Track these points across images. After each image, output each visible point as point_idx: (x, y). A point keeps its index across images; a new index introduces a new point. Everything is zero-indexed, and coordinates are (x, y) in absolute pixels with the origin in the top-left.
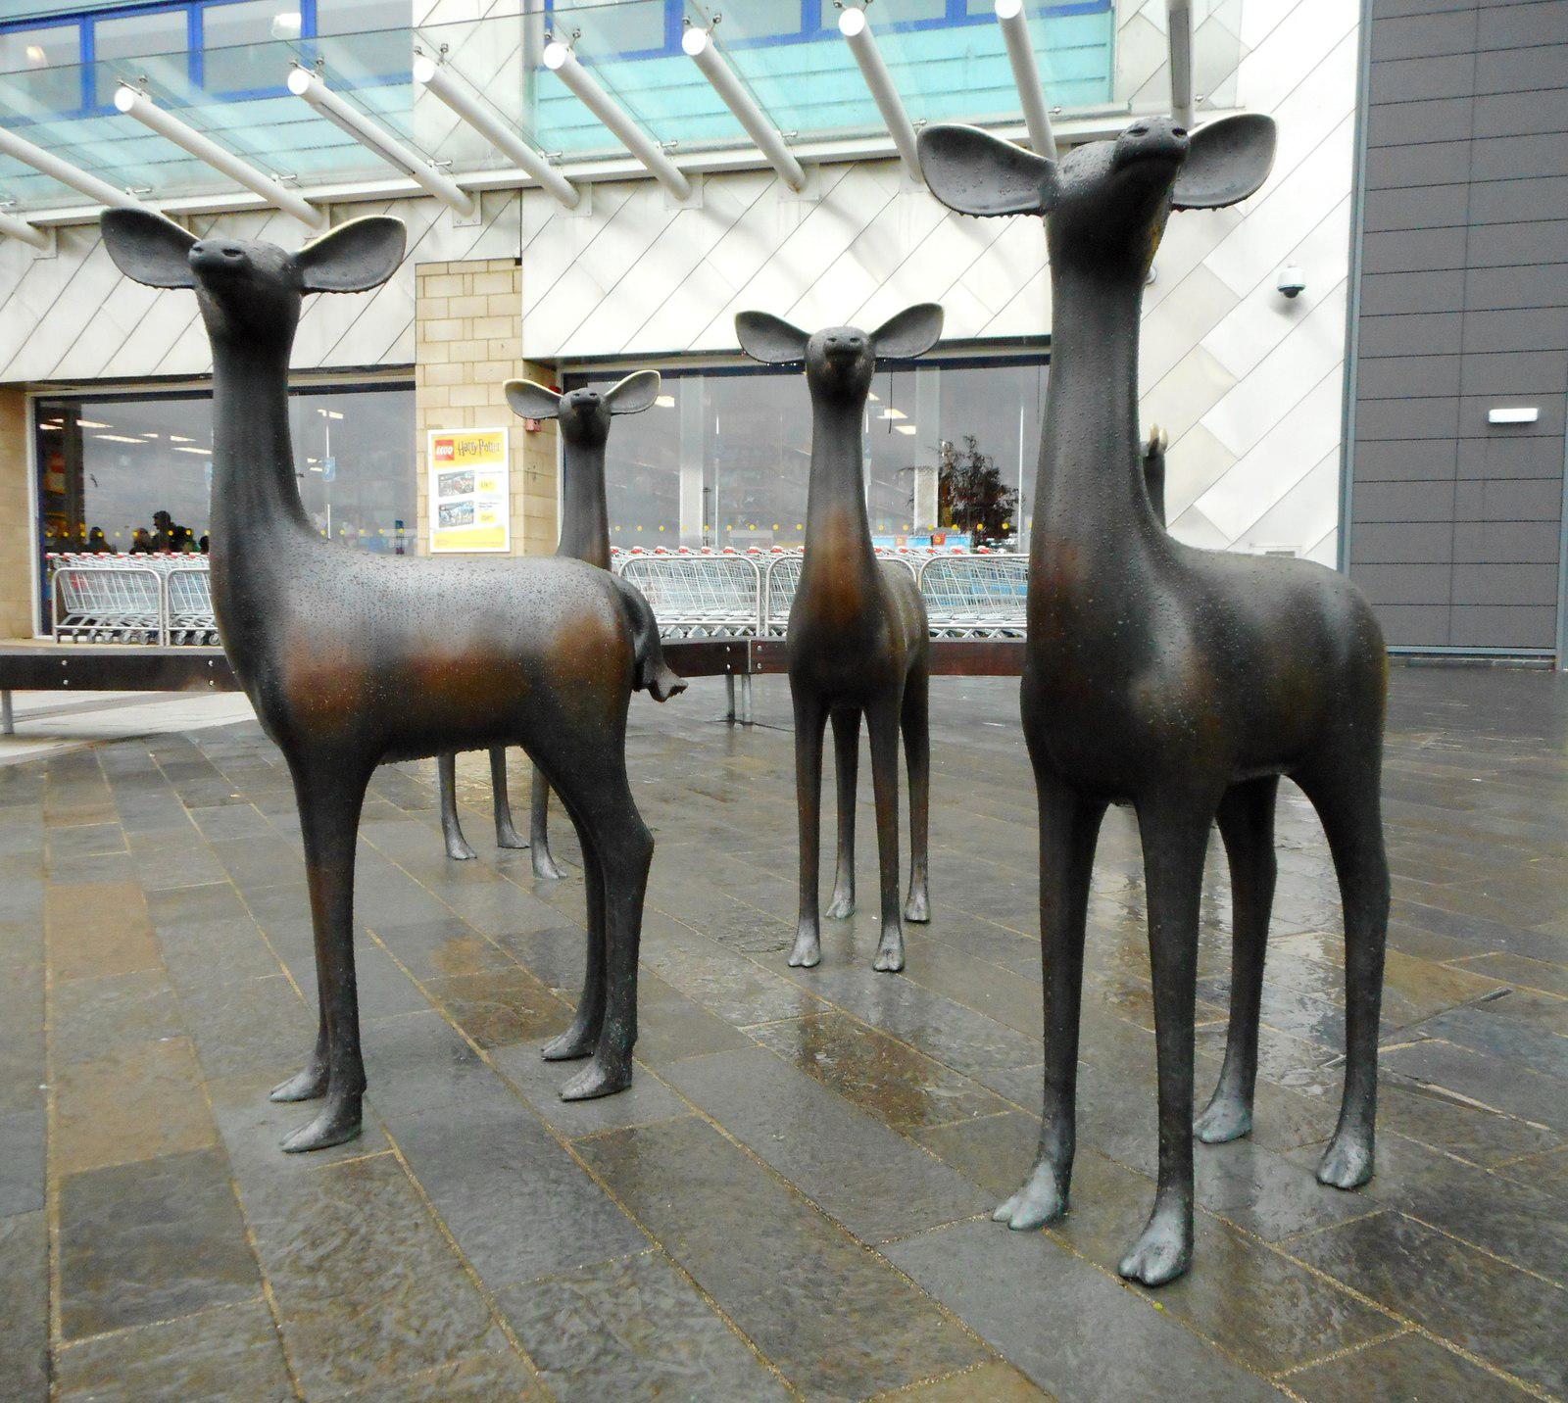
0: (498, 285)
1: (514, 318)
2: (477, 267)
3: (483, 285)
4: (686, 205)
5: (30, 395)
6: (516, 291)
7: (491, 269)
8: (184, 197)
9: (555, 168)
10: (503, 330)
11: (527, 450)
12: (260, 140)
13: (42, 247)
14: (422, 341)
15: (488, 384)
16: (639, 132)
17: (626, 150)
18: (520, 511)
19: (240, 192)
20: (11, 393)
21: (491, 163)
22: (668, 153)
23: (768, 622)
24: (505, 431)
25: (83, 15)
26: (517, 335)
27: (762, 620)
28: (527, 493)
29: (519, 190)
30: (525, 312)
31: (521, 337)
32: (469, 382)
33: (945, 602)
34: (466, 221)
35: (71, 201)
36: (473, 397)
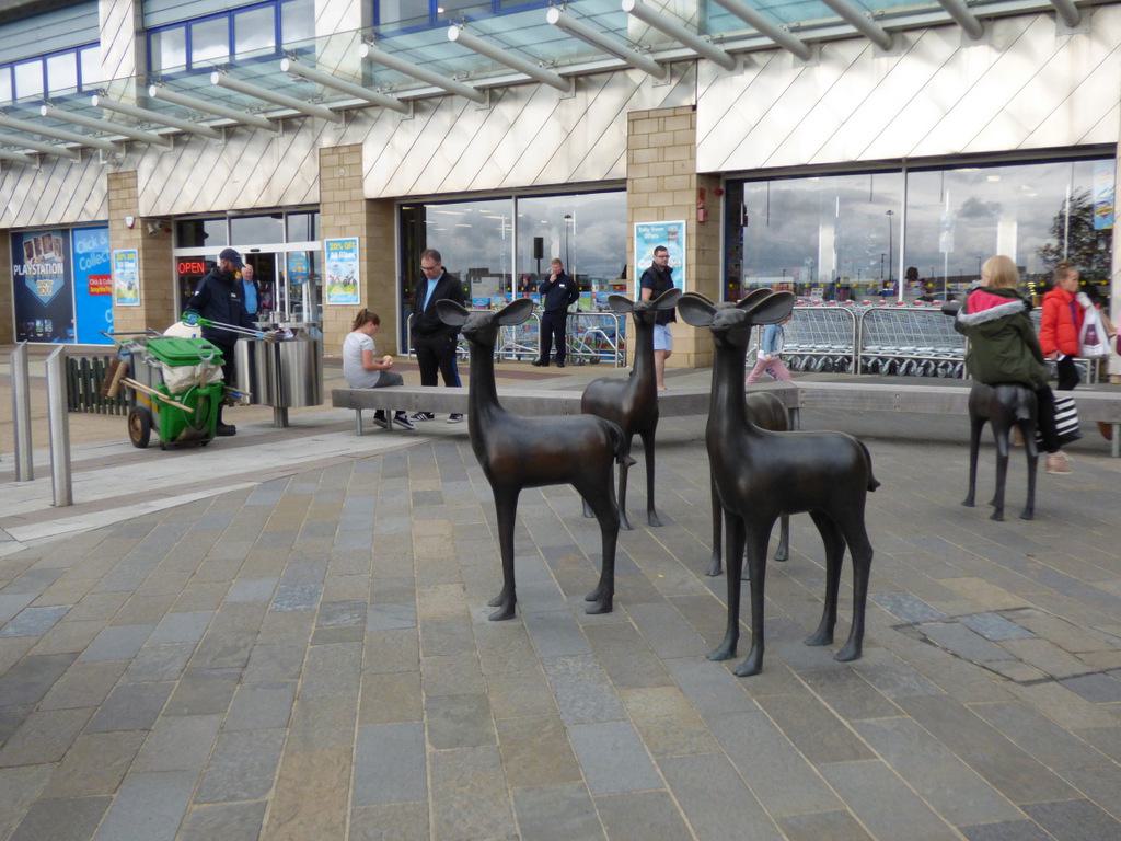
0: (682, 124)
1: (691, 146)
2: (667, 113)
3: (672, 125)
4: (1075, 30)
5: (722, 180)
6: (693, 128)
7: (672, 111)
8: (487, 77)
9: (876, 23)
10: (683, 154)
11: (698, 234)
12: (521, 38)
13: (406, 112)
14: (631, 163)
15: (673, 191)
16: (763, 17)
17: (838, 18)
18: (693, 275)
19: (425, 87)
20: (4, 231)
21: (666, 45)
22: (794, 30)
23: (861, 354)
24: (684, 222)
25: (230, 11)
26: (693, 157)
27: (857, 351)
28: (698, 263)
29: (696, 60)
30: (697, 143)
31: (695, 159)
32: (661, 190)
33: (875, 338)
34: (482, 106)
35: (418, 85)
36: (663, 200)
